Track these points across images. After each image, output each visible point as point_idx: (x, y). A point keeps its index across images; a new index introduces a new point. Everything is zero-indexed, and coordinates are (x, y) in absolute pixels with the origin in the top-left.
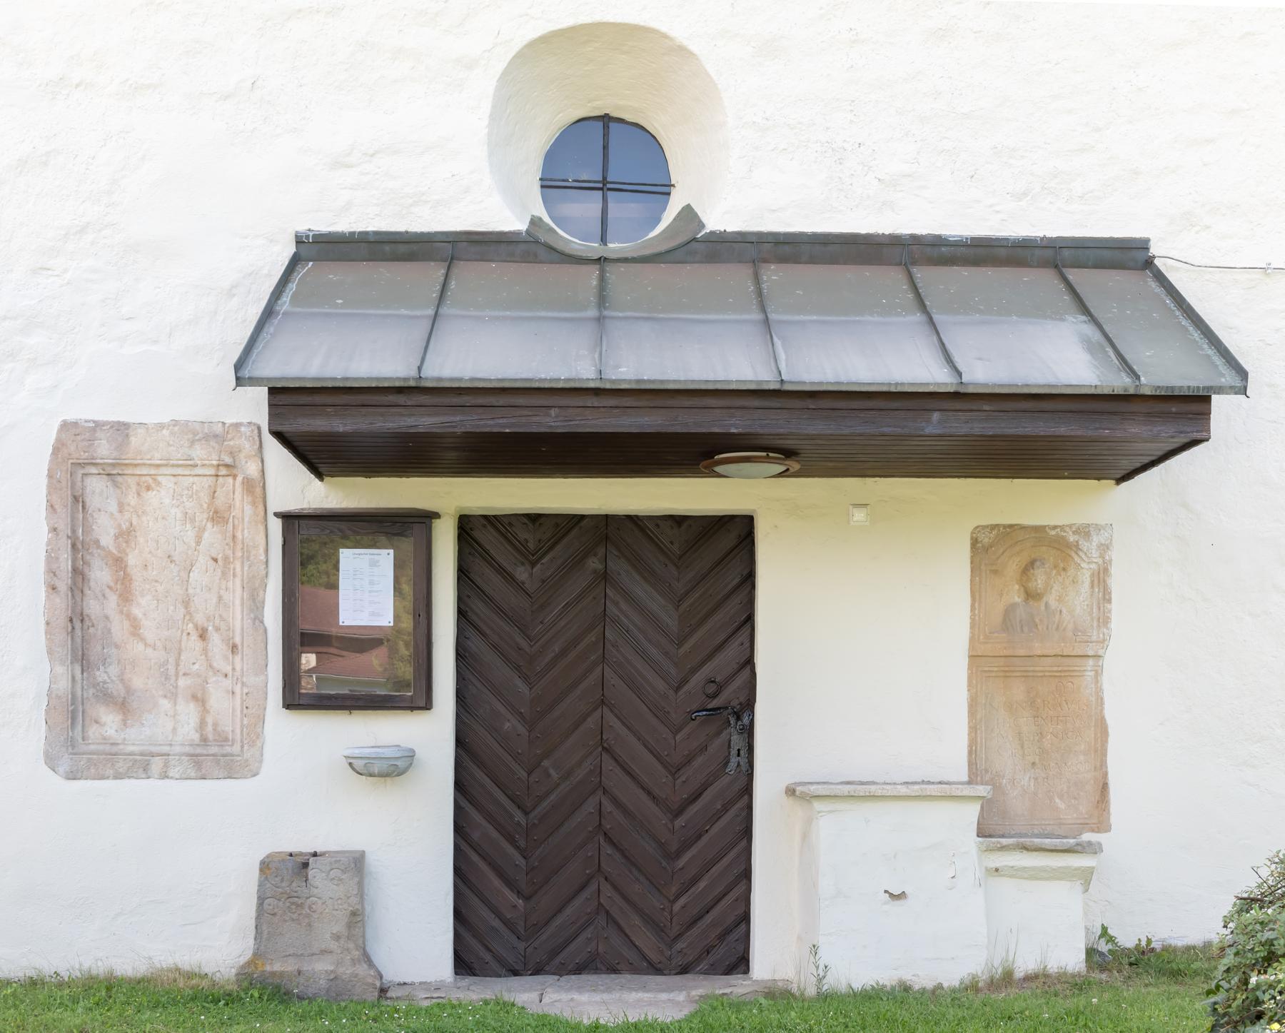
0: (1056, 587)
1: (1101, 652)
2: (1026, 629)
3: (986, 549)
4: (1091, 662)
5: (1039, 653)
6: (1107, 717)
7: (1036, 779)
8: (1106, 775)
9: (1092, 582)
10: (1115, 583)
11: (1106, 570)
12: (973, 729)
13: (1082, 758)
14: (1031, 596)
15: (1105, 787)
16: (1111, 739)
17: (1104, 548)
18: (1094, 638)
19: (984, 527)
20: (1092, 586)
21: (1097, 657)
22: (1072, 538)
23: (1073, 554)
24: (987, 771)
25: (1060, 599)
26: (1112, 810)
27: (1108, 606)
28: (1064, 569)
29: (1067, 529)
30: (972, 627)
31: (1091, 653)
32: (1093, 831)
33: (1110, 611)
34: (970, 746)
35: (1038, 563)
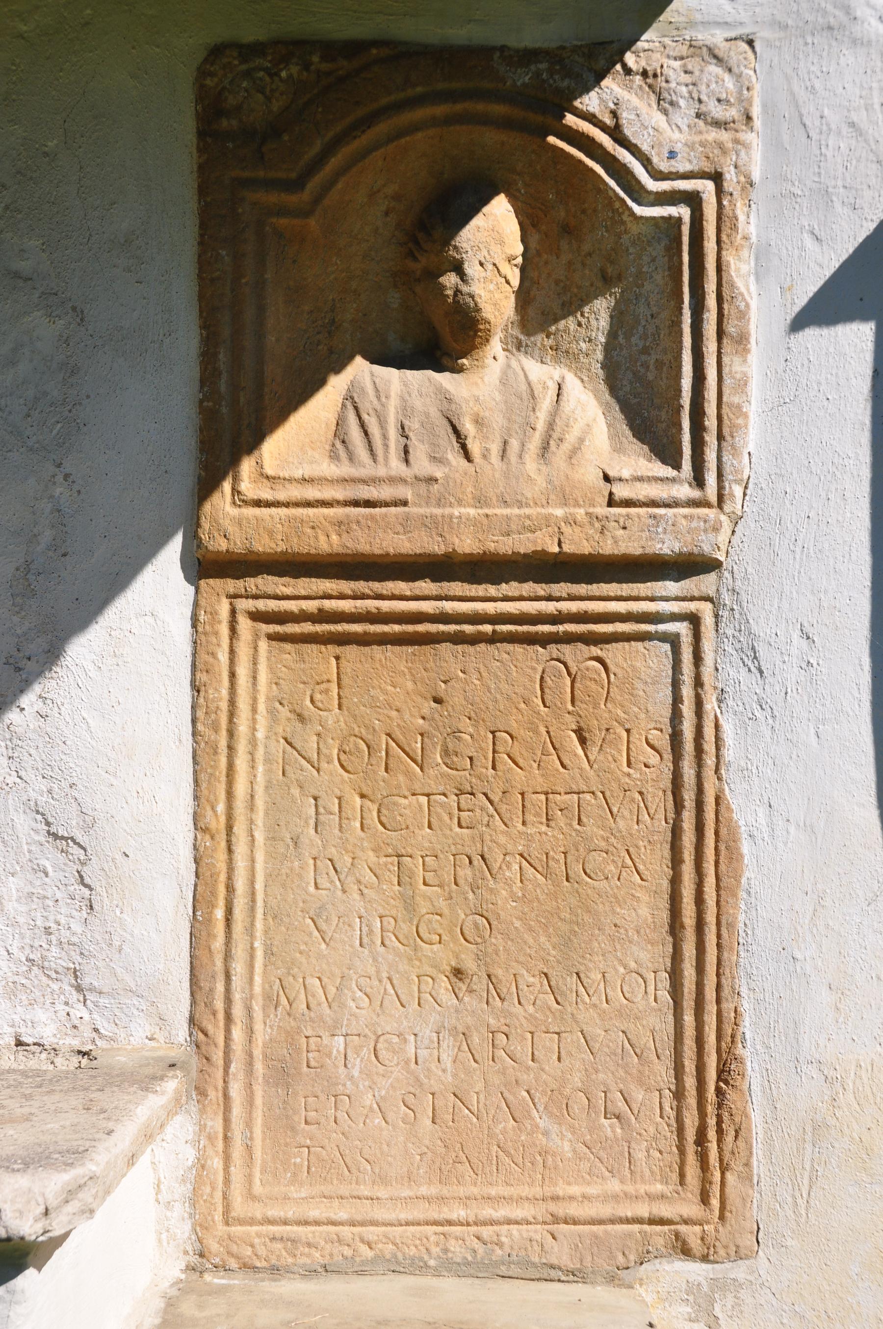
2: (419, 452)
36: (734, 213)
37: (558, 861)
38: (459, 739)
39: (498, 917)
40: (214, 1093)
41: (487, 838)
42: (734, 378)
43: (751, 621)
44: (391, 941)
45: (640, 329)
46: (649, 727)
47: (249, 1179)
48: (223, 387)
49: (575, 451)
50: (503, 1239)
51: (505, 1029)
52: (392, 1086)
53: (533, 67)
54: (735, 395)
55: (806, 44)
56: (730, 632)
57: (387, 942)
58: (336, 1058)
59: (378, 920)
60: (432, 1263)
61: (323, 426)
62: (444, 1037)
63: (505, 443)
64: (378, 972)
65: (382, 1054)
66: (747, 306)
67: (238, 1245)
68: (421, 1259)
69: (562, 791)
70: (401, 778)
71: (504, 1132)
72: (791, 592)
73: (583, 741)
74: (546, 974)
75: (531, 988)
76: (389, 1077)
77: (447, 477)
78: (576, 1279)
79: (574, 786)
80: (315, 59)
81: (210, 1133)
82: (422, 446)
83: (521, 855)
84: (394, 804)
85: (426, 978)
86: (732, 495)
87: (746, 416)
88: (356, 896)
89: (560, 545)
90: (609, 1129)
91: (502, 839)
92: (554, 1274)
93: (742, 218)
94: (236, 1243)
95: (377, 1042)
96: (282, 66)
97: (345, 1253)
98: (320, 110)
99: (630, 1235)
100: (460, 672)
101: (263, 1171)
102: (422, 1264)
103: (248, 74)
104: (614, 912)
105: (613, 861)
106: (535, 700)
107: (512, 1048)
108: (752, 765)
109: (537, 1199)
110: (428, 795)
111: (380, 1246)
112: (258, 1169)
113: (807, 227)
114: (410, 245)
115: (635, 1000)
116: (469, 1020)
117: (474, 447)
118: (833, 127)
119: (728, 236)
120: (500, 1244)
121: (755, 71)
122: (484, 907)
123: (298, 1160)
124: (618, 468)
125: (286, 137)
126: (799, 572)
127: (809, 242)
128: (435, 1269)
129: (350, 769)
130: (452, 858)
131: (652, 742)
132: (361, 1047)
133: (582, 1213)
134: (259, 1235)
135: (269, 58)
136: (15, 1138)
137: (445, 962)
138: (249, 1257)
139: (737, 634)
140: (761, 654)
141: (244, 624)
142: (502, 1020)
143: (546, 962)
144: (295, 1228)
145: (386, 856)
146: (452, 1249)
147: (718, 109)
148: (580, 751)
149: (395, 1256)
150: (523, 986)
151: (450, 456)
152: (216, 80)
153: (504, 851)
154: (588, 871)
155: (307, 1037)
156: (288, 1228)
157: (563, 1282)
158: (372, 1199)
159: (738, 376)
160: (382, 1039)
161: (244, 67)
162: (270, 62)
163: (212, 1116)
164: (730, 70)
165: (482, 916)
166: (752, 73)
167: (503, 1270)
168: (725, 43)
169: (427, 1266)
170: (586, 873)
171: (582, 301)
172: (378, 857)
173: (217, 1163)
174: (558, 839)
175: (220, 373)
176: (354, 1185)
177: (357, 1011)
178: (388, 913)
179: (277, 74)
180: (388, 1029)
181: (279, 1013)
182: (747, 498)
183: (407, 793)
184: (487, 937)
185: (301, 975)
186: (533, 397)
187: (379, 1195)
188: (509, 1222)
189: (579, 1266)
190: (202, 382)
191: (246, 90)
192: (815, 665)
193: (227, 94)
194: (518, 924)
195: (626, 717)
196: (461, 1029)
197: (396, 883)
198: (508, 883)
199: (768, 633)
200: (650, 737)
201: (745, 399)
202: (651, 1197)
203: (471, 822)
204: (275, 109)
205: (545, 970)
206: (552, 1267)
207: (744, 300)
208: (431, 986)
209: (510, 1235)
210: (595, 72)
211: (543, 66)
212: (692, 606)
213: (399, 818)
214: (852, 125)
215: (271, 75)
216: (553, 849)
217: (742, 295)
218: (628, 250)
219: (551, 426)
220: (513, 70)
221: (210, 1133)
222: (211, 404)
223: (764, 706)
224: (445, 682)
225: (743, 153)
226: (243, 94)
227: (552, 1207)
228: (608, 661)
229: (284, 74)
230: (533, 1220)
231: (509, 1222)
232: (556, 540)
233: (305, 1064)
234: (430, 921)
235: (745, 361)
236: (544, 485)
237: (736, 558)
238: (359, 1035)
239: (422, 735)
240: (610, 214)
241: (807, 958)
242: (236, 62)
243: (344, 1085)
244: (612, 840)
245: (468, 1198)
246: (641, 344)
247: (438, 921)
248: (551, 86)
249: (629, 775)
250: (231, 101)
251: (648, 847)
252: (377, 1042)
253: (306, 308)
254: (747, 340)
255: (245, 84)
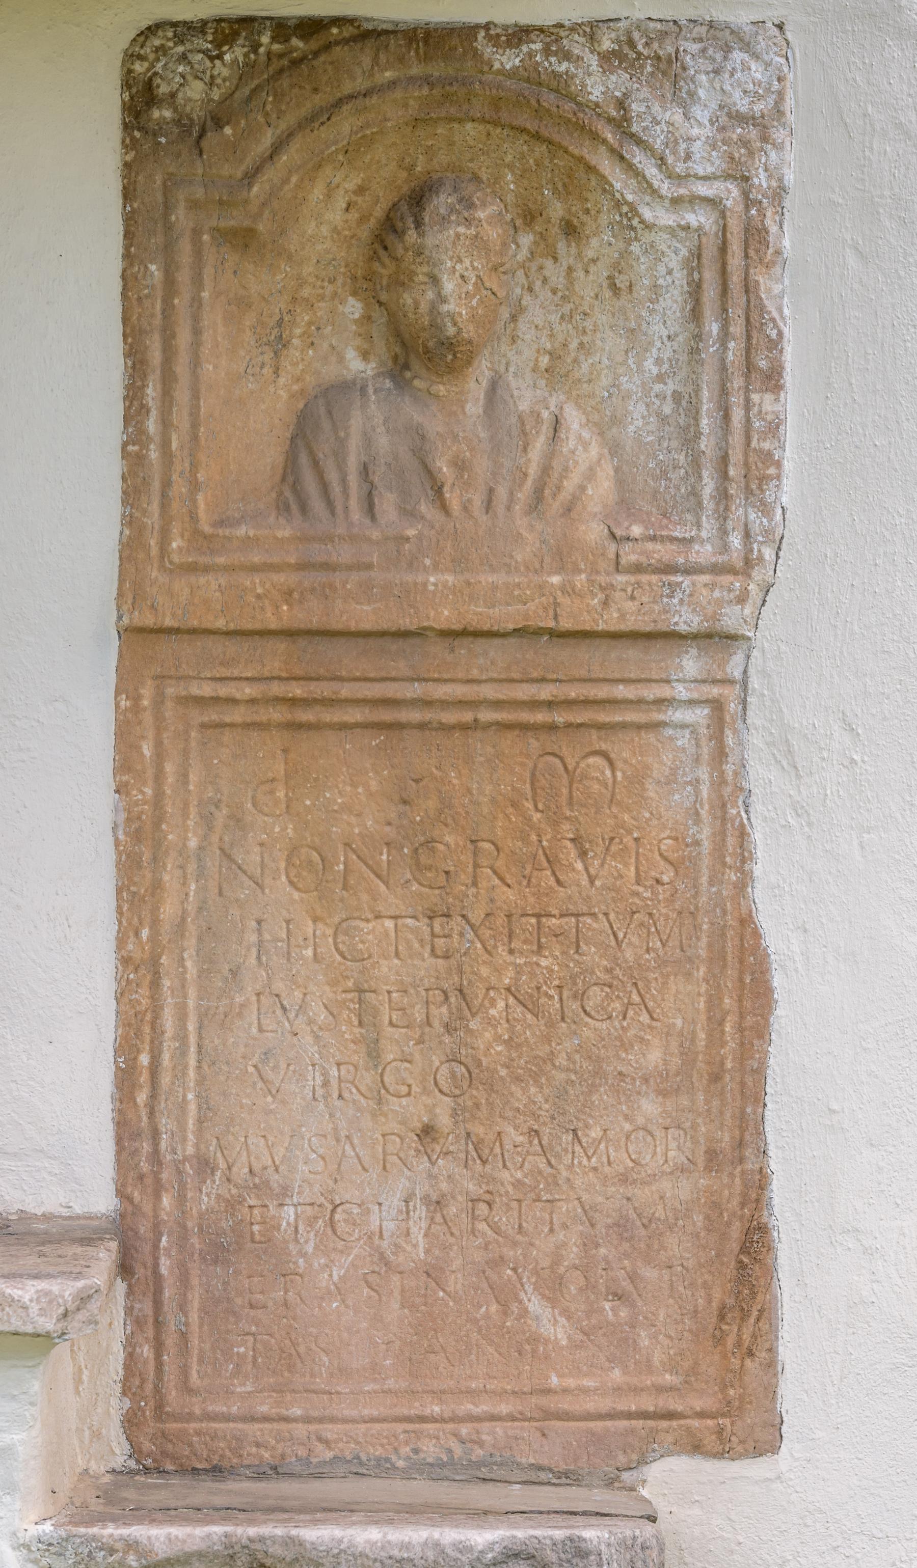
0: (538, 312)
1: (732, 618)
2: (387, 503)
3: (196, 132)
4: (690, 664)
5: (445, 616)
6: (765, 920)
7: (438, 1204)
8: (757, 1188)
9: (695, 290)
10: (791, 303)
11: (756, 237)
12: (140, 972)
13: (649, 1107)
14: (420, 353)
15: (748, 1252)
16: (783, 1016)
17: (751, 130)
18: (704, 553)
19: (185, 30)
20: (696, 314)
21: (717, 639)
22: (597, 85)
23: (606, 165)
24: (205, 1166)
25: (556, 370)
26: (786, 1352)
27: (765, 401)
28: (570, 230)
29: (577, 45)
30: (132, 492)
31: (685, 620)
32: (696, 1448)
33: (774, 428)
34: (126, 1048)
35: (442, 201)
36: (763, 225)
37: (551, 997)
38: (433, 850)
39: (479, 1064)
40: (142, 1270)
41: (466, 968)
42: (764, 420)
43: (785, 710)
44: (351, 1093)
45: (654, 350)
46: (663, 835)
47: (185, 1371)
48: (152, 425)
49: (568, 510)
50: (484, 1437)
51: (487, 1197)
52: (352, 1264)
53: (525, 48)
54: (764, 440)
55: (845, 32)
56: (758, 722)
57: (346, 1095)
58: (286, 1231)
59: (335, 1069)
60: (401, 1464)
61: (268, 468)
62: (415, 1207)
63: (491, 491)
64: (335, 1129)
65: (341, 1227)
66: (780, 334)
67: (174, 1444)
68: (387, 1460)
69: (556, 912)
70: (365, 897)
71: (487, 1316)
72: (832, 676)
73: (583, 854)
74: (536, 1131)
75: (519, 1149)
76: (349, 1255)
77: (420, 537)
78: (568, 1481)
79: (571, 907)
80: (265, 39)
81: (138, 1317)
82: (389, 495)
83: (508, 990)
84: (356, 928)
85: (393, 1137)
86: (761, 558)
87: (778, 464)
88: (309, 1039)
89: (556, 617)
90: (610, 1313)
91: (485, 971)
92: (544, 1476)
93: (773, 229)
94: (171, 1441)
95: (333, 1211)
96: (225, 48)
97: (300, 1453)
98: (270, 99)
99: (633, 1431)
100: (434, 770)
101: (201, 1361)
102: (388, 1465)
103: (183, 58)
104: (618, 1056)
105: (618, 997)
106: (526, 804)
107: (496, 1219)
108: (785, 882)
109: (524, 1393)
110: (395, 918)
111: (340, 1445)
112: (195, 1359)
113: (850, 242)
114: (376, 245)
115: (643, 1162)
116: (444, 1186)
117: (453, 497)
118: (878, 126)
119: (757, 251)
120: (481, 1444)
121: (787, 59)
122: (463, 1052)
123: (242, 1350)
124: (626, 524)
125: (228, 130)
126: (841, 652)
127: (852, 260)
128: (404, 1471)
129: (300, 886)
130: (424, 993)
131: (665, 854)
132: (316, 1218)
133: (577, 1407)
134: (198, 1433)
135: (210, 38)
136: (6, 1269)
137: (415, 1118)
138: (187, 1457)
139: (767, 725)
140: (796, 747)
141: (169, 710)
142: (483, 1186)
143: (536, 1118)
144: (240, 1426)
145: (344, 992)
146: (425, 1448)
147: (744, 102)
148: (579, 866)
149: (358, 1458)
150: (508, 1146)
151: (423, 508)
152: (146, 64)
153: (487, 985)
154: (588, 1009)
155: (250, 1207)
156: (231, 1425)
157: (554, 1484)
158: (331, 1393)
159: (769, 417)
160: (339, 1209)
161: (180, 49)
162: (211, 42)
163: (141, 1297)
164: (758, 57)
165: (460, 1063)
166: (783, 61)
167: (484, 1472)
168: (750, 27)
169: (395, 1468)
170: (585, 1011)
171: (585, 314)
172: (335, 992)
173: (146, 1351)
174: (552, 971)
175: (148, 412)
176: (307, 1378)
177: (312, 1176)
178: (347, 1059)
179: (220, 57)
180: (347, 1197)
181: (217, 1178)
182: (780, 561)
183: (370, 916)
184: (465, 1088)
185: (243, 1134)
186: (524, 433)
187: (339, 1389)
188: (493, 1418)
189: (572, 1467)
190: (127, 419)
191: (183, 76)
192: (860, 763)
193: (159, 81)
194: (503, 1072)
195: (635, 823)
196: (434, 1198)
197: (356, 1023)
198: (490, 1022)
199: (805, 723)
200: (663, 847)
201: (777, 444)
202: (661, 1389)
203: (447, 951)
204: (216, 98)
205: (536, 1127)
206: (540, 1468)
207: (776, 326)
208: (398, 1147)
209: (492, 1433)
210: (599, 54)
211: (537, 46)
212: (715, 691)
213: (360, 946)
214: (899, 126)
215: (212, 59)
216: (546, 983)
217: (773, 320)
218: (639, 259)
219: (546, 470)
220: (500, 51)
221: (138, 1317)
222: (136, 448)
223: (800, 811)
224: (417, 781)
225: (773, 155)
226: (178, 79)
227: (543, 1401)
228: (613, 756)
229: (227, 57)
230: (519, 1416)
231: (493, 1418)
232: (551, 613)
233: (249, 1239)
234: (398, 1069)
235: (777, 400)
236: (538, 545)
237: (767, 633)
238: (312, 1204)
239: (387, 844)
240: (618, 218)
241: (846, 1110)
242: (171, 44)
243: (295, 1263)
244: (618, 972)
245: (443, 1392)
246: (655, 371)
247: (406, 1069)
248: (546, 69)
249: (637, 894)
250: (163, 89)
251: (660, 980)
252: (333, 1211)
253: (248, 323)
254: (780, 375)
255: (181, 69)
